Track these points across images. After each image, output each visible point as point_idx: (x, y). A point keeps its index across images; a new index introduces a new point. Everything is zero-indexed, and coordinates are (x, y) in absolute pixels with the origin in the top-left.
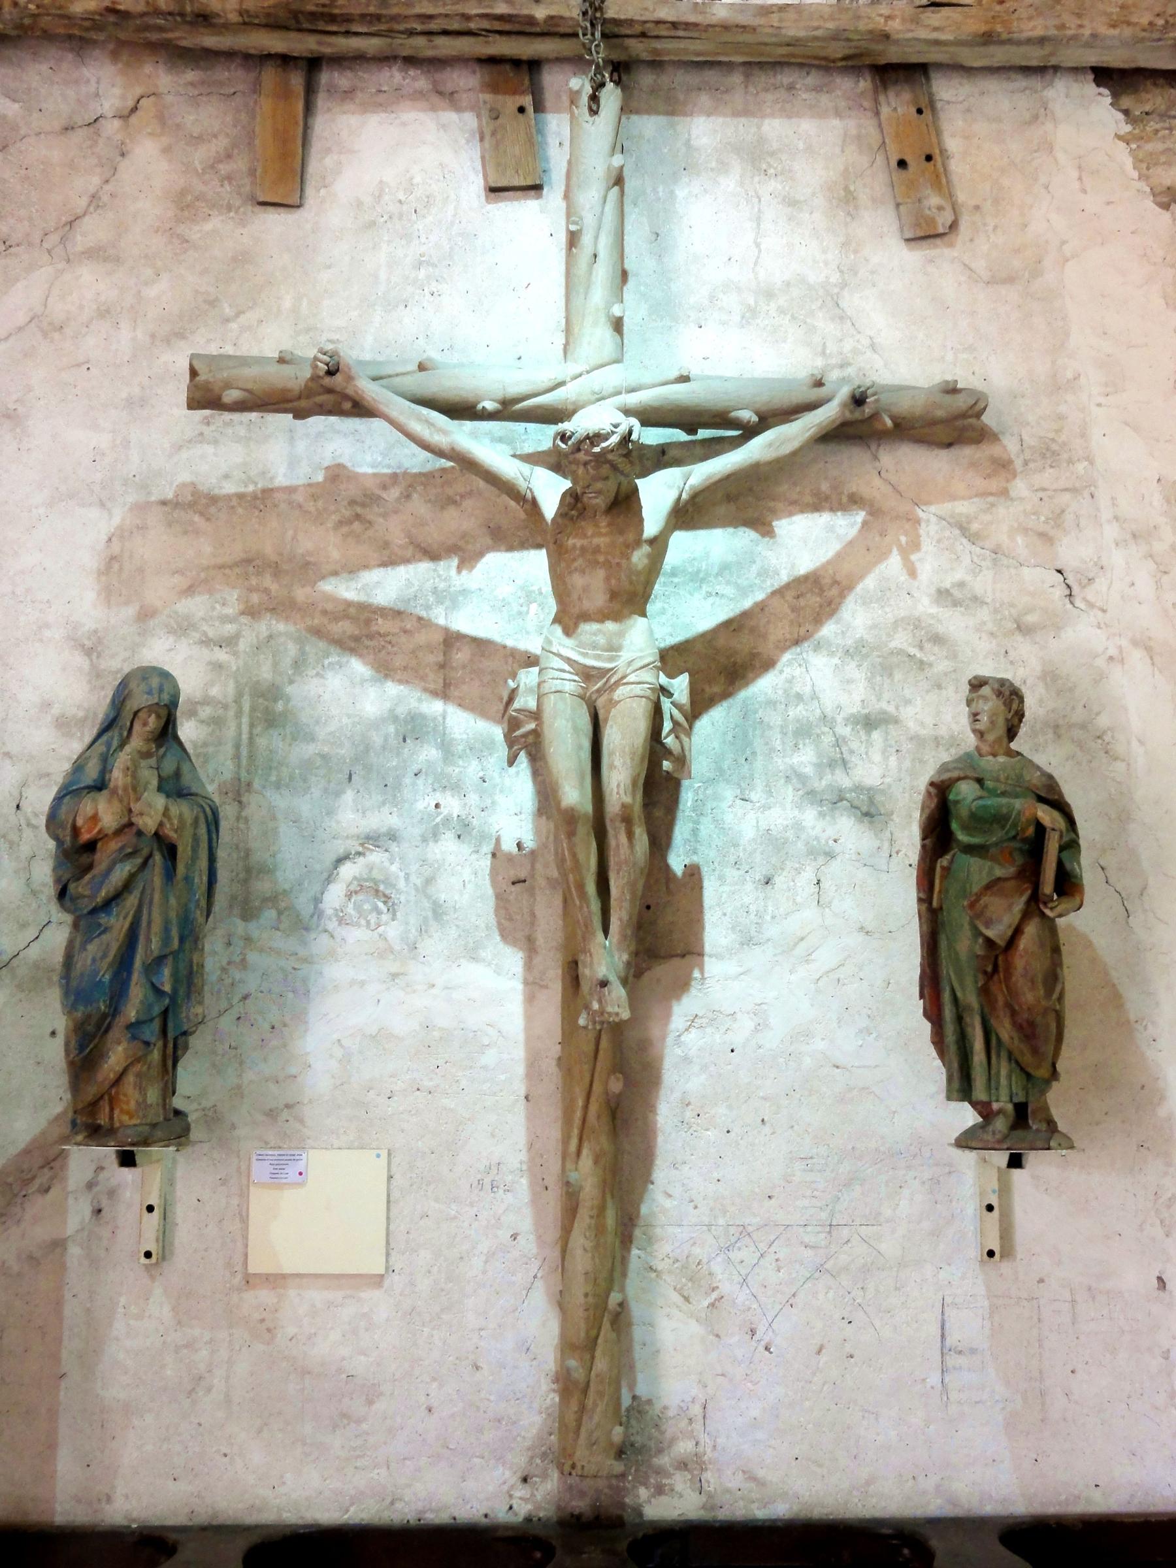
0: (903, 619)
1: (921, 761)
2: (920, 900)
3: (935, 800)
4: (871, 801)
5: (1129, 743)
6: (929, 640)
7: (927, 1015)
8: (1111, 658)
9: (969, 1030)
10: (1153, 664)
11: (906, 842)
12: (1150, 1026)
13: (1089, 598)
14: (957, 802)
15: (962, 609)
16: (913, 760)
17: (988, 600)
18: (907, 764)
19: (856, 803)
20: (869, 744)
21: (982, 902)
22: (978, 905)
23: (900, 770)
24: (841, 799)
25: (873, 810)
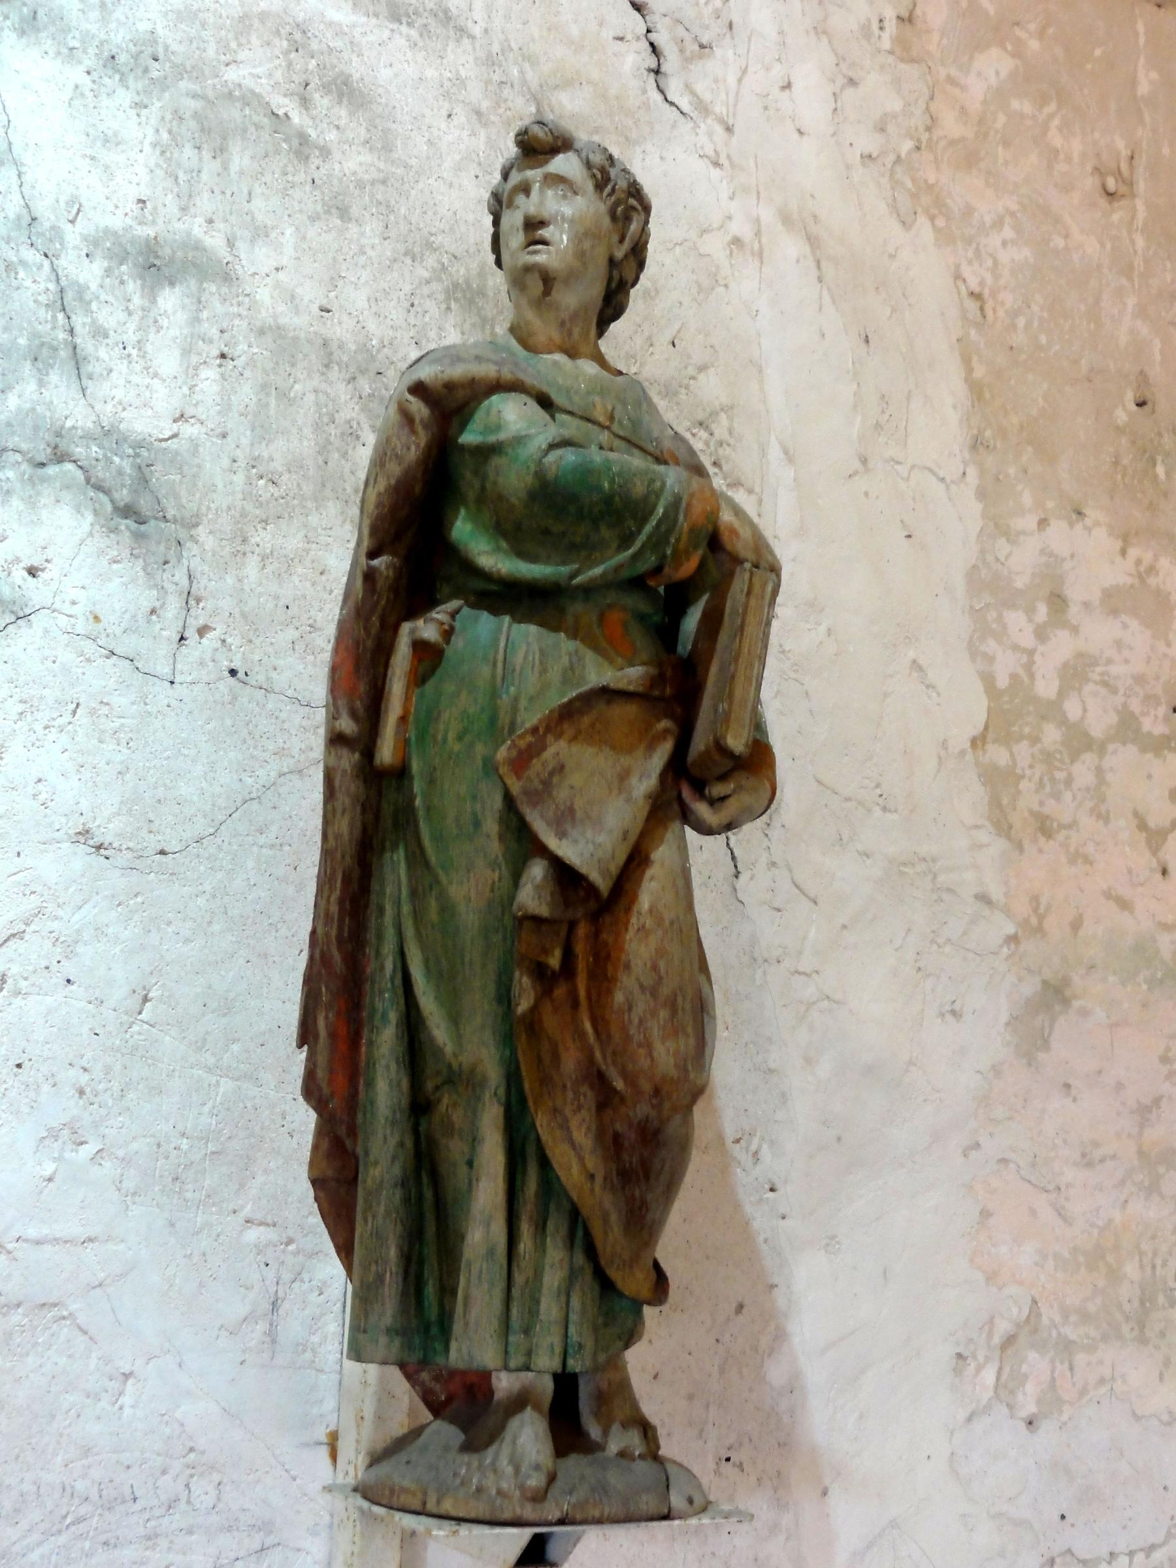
0: (263, 16)
1: (283, 395)
2: (336, 740)
3: (423, 438)
4: (142, 478)
5: (763, 453)
6: (326, 88)
7: (311, 1090)
8: (737, 241)
9: (455, 1149)
10: (820, 279)
11: (227, 604)
12: (765, 1152)
13: (700, 88)
14: (486, 452)
15: (414, 33)
16: (264, 387)
17: (477, 30)
18: (246, 393)
19: (100, 473)
20: (150, 322)
21: (548, 754)
22: (536, 764)
23: (225, 408)
24: (60, 457)
25: (145, 504)
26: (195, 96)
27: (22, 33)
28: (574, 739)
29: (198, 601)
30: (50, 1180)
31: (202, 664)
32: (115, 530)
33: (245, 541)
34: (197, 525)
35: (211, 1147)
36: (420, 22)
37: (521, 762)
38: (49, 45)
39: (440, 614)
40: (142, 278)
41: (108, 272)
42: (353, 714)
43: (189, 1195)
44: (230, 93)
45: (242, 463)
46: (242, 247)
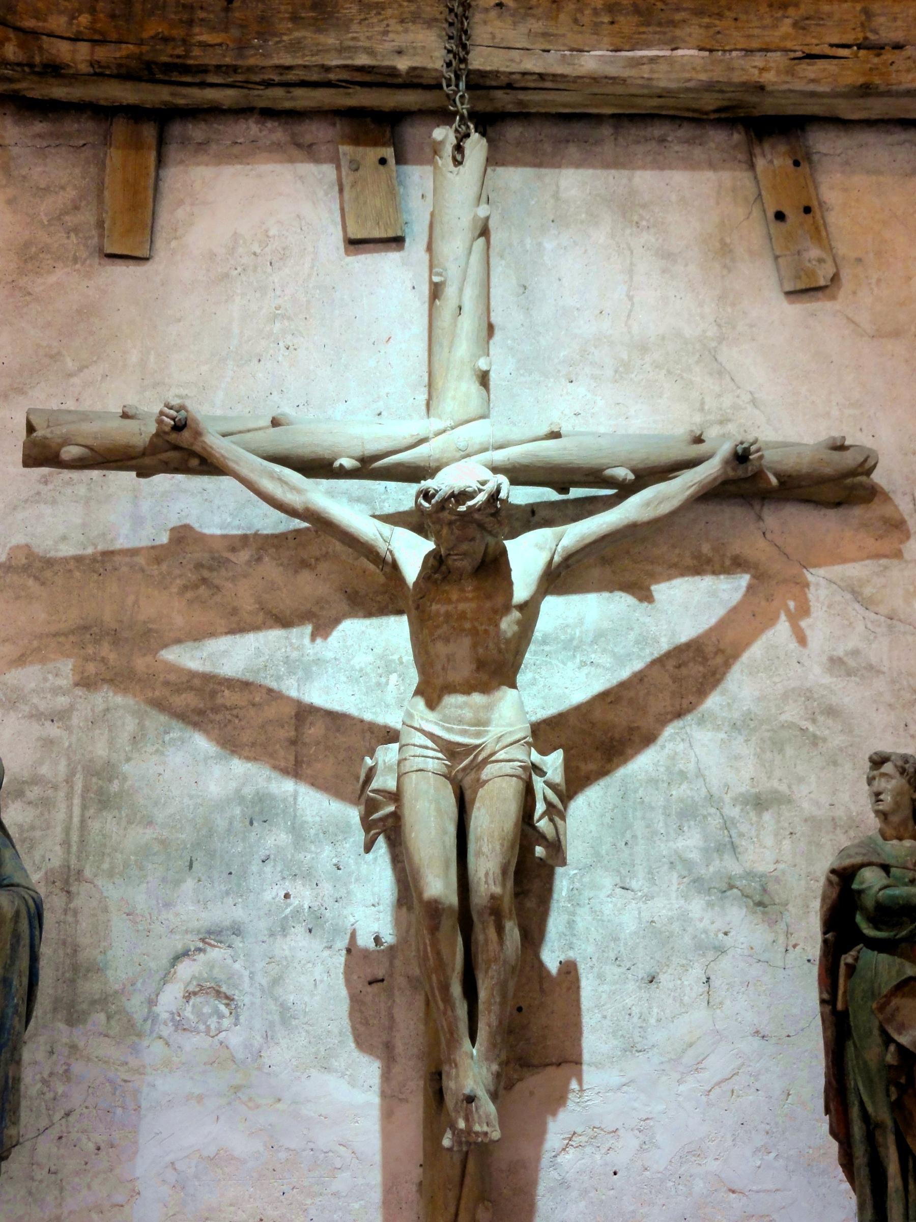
0: (793, 689)
1: (818, 845)
2: (823, 1002)
4: (765, 890)
6: (822, 713)
7: (833, 1133)
14: (860, 892)
15: (857, 679)
16: (810, 843)
17: (885, 669)
19: (748, 891)
24: (731, 887)
25: (766, 900)
26: (768, 731)
27: (699, 724)
28: (903, 996)
29: (792, 934)
30: (759, 1167)
31: (796, 959)
32: (755, 912)
33: (808, 907)
34: (787, 905)
35: (822, 1151)
36: (860, 673)
37: (882, 1008)
38: (709, 726)
39: (853, 953)
40: (755, 809)
41: (742, 810)
42: (827, 992)
43: (815, 1171)
44: (783, 726)
45: (803, 876)
46: (794, 788)
